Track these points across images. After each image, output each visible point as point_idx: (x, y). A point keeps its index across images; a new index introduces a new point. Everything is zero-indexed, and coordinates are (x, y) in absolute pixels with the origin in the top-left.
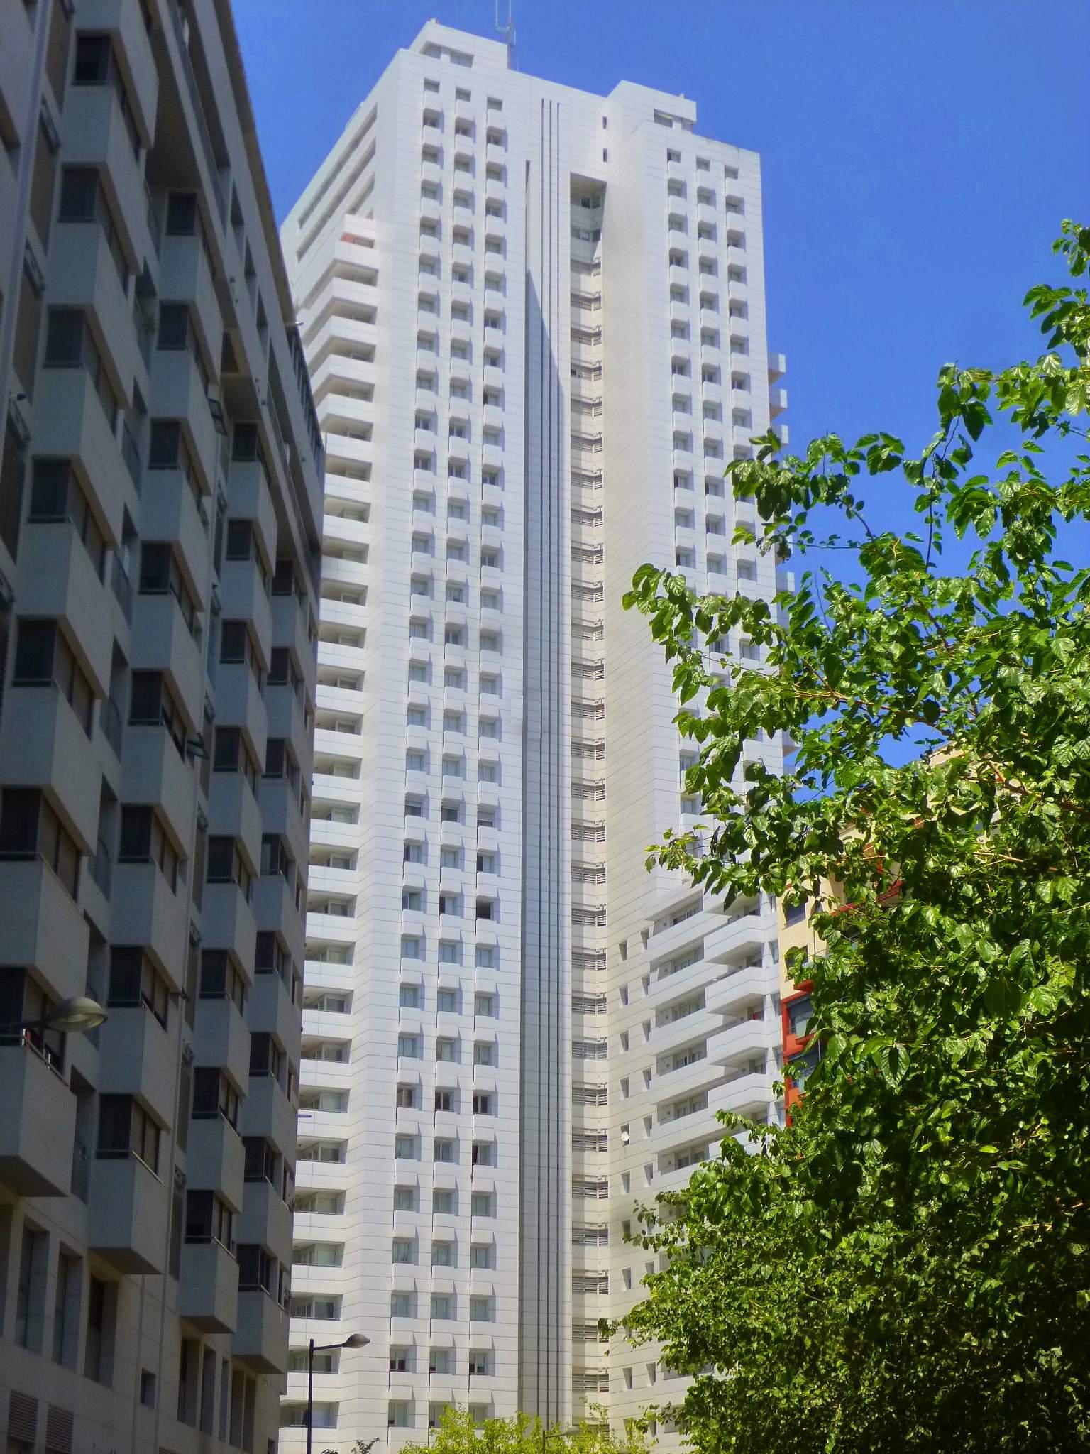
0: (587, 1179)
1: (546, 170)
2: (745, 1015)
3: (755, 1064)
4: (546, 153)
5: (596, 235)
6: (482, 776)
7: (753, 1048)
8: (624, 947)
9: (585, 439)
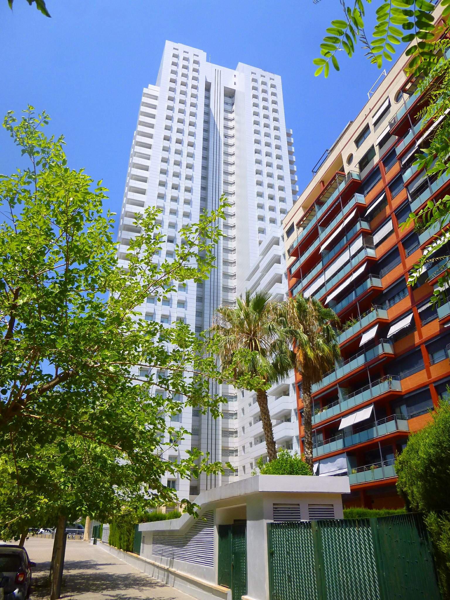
2: (282, 394)
3: (287, 418)
5: (233, 104)
8: (243, 410)
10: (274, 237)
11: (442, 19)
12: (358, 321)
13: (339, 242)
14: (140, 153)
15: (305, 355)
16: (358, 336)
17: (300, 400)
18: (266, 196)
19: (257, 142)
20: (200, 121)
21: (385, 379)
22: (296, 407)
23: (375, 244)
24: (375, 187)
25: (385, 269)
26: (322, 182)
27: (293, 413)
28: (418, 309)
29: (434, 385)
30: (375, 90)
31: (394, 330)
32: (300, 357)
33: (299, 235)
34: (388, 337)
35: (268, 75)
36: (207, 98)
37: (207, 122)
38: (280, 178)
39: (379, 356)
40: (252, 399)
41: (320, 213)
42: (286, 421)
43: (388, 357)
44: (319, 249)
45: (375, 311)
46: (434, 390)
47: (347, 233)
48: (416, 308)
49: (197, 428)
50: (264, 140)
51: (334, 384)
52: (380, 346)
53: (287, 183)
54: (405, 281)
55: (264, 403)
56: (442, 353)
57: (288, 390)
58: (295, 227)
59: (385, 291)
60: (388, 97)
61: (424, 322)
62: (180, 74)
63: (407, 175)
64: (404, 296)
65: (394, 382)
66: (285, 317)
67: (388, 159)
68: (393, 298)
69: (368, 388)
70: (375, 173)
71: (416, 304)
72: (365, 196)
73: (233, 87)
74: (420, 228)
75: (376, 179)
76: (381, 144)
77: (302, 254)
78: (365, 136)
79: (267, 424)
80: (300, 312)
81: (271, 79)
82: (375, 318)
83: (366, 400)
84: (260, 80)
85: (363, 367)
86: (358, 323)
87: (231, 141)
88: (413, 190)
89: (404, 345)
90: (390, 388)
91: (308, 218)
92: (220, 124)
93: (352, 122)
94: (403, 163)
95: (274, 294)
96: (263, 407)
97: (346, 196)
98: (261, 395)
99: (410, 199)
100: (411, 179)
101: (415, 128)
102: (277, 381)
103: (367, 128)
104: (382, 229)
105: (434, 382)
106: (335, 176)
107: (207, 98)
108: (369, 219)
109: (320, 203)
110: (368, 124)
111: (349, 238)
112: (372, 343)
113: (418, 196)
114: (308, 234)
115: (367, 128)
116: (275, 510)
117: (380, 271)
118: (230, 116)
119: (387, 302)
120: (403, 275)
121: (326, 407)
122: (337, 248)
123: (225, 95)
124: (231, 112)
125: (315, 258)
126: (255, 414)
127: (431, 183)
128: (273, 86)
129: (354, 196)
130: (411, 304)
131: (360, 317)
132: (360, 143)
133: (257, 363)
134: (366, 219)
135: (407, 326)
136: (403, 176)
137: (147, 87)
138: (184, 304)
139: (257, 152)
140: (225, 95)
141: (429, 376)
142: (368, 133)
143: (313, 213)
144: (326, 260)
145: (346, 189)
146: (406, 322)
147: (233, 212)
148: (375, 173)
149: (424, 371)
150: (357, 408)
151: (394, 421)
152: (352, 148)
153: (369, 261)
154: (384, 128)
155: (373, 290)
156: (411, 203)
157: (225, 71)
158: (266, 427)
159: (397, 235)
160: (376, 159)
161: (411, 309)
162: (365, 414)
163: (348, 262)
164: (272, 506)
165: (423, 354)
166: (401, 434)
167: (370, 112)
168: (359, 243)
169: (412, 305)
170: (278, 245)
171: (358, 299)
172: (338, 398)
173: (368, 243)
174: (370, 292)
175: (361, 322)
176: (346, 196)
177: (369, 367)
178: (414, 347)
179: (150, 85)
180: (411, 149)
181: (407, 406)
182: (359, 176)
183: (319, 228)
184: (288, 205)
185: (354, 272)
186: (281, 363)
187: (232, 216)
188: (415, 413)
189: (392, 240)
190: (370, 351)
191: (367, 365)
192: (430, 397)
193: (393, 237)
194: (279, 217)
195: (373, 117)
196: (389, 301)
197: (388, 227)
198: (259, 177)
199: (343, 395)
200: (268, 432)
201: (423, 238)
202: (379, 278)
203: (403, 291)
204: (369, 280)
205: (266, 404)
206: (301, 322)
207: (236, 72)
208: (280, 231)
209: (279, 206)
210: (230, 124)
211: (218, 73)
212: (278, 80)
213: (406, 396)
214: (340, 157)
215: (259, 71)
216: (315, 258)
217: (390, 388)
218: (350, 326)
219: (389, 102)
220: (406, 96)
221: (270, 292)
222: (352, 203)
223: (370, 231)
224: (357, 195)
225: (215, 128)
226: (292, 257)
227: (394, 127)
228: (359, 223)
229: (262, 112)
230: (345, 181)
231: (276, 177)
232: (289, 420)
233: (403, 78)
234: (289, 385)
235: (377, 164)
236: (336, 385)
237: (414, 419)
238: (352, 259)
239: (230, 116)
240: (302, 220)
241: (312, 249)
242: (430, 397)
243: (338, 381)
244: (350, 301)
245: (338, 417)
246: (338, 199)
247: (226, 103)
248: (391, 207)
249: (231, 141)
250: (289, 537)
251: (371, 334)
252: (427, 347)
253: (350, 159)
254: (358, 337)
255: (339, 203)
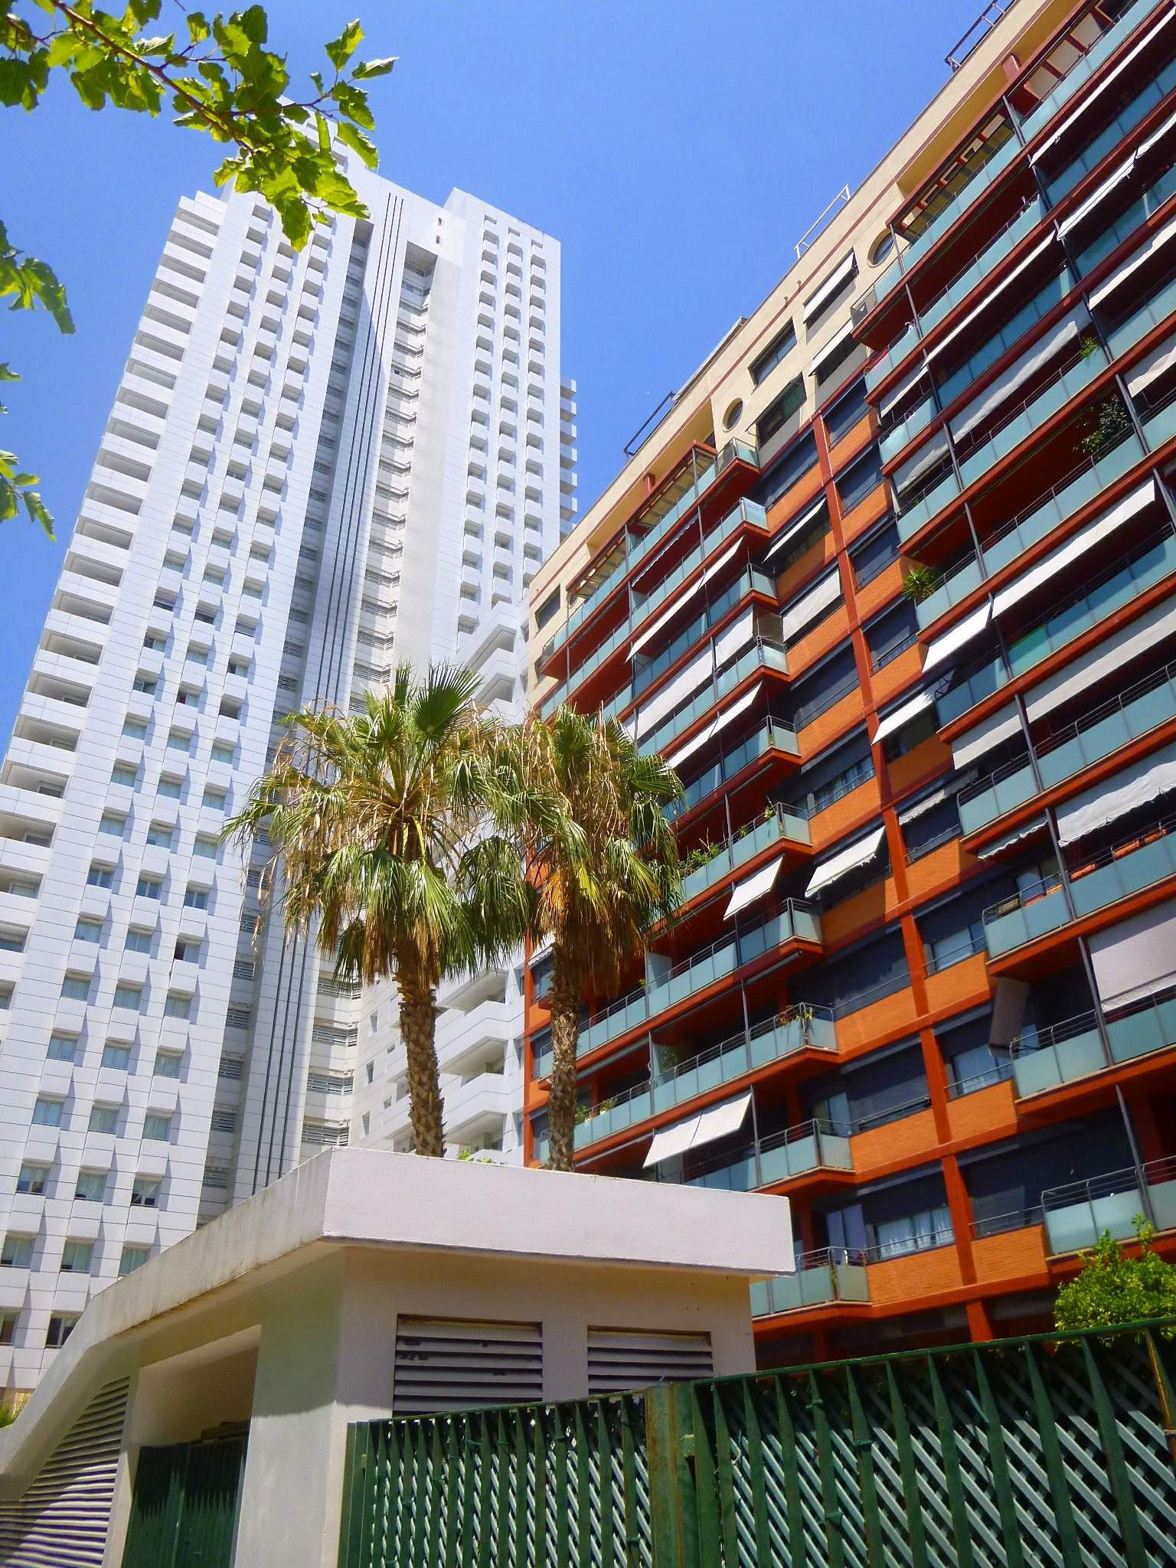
0: (336, 1025)
1: (325, 672)
2: (481, 1142)
3: (493, 1064)
4: (325, 672)
5: (426, 292)
6: (159, 1070)
7: (485, 1113)
8: (366, 1119)
9: (380, 606)
10: (500, 629)
11: (1010, 54)
12: (722, 848)
13: (686, 629)
14: (145, 366)
15: (572, 890)
16: (721, 891)
17: (534, 1085)
18: (489, 535)
19: (481, 392)
20: (331, 309)
21: (791, 1016)
22: (519, 1104)
23: (785, 639)
24: (794, 489)
25: (812, 706)
26: (651, 476)
27: (510, 1125)
28: (899, 815)
29: (933, 1032)
30: (814, 239)
31: (824, 875)
32: (555, 900)
33: (571, 617)
34: (807, 895)
35: (529, 232)
36: (358, 261)
37: (348, 323)
38: (533, 495)
39: (778, 948)
40: (395, 1086)
41: (636, 554)
42: (486, 1147)
43: (806, 952)
44: (626, 649)
45: (775, 820)
46: (935, 1046)
47: (712, 603)
48: (895, 813)
49: (223, 1165)
50: (494, 496)
51: (639, 1032)
52: (784, 917)
53: (550, 483)
54: (866, 735)
55: (421, 1031)
56: (963, 939)
57: (501, 1058)
58: (564, 594)
59: (808, 767)
60: (852, 250)
61: (914, 853)
62: (299, 283)
63: (894, 444)
64: (862, 780)
65: (817, 1023)
66: (517, 769)
67: (836, 414)
68: (829, 787)
69: (741, 1042)
70: (803, 447)
71: (895, 799)
72: (767, 511)
73: (431, 247)
74: (923, 585)
75: (801, 463)
76: (823, 372)
77: (576, 665)
78: (780, 354)
79: (426, 1102)
80: (565, 758)
81: (533, 243)
82: (775, 837)
83: (730, 1078)
84: (506, 240)
85: (730, 981)
86: (724, 855)
87: (409, 385)
88: (906, 483)
89: (852, 919)
90: (807, 1042)
91: (602, 572)
92: (387, 337)
93: (744, 321)
94: (884, 413)
95: (488, 679)
96: (417, 1042)
97: (716, 507)
98: (415, 1005)
99: (897, 509)
100: (903, 454)
101: (924, 320)
102: (473, 964)
103: (788, 332)
104: (807, 599)
105: (936, 1025)
106: (691, 452)
107: (358, 261)
108: (775, 569)
109: (637, 527)
110: (791, 322)
111: (714, 620)
112: (761, 912)
113: (921, 498)
114: (599, 611)
115: (788, 332)
116: (408, 1350)
117: (795, 710)
118: (416, 321)
119: (811, 797)
120: (864, 720)
121: (611, 1101)
122: (679, 647)
123: (407, 265)
124: (420, 312)
125: (616, 675)
126: (398, 1133)
127: (961, 463)
128: (537, 262)
129: (738, 504)
130: (878, 802)
131: (731, 838)
132: (764, 374)
133: (411, 886)
134: (765, 569)
135: (867, 860)
136: (881, 447)
137: (192, 197)
138: (223, 798)
139: (478, 418)
140: (408, 265)
141: (922, 1005)
142: (790, 343)
143: (618, 556)
144: (643, 682)
145: (716, 489)
146: (864, 851)
147: (393, 571)
148: (803, 447)
149: (909, 991)
150: (700, 1103)
151: (810, 1140)
152: (741, 385)
153: (767, 678)
154: (839, 325)
155: (774, 759)
156: (900, 517)
157: (415, 204)
158: (423, 1112)
159: (852, 612)
160: (807, 412)
161: (880, 815)
162: (729, 1119)
163: (708, 683)
164: (390, 1328)
165: (907, 944)
166: (830, 1177)
167: (800, 290)
168: (743, 630)
169: (882, 805)
170: (509, 699)
171: (730, 787)
172: (647, 1075)
173: (768, 630)
174: (765, 765)
175: (731, 853)
176: (716, 507)
177: (745, 980)
178: (881, 922)
179: (200, 194)
180: (907, 377)
181: (849, 1099)
182: (756, 455)
183: (632, 595)
184: (547, 538)
185: (723, 711)
186: (492, 906)
187: (389, 580)
188: (873, 1116)
189: (838, 625)
190: (750, 935)
191: (741, 974)
192: (920, 1070)
193: (841, 617)
194: (521, 566)
195: (806, 304)
196: (817, 797)
197: (830, 589)
198: (475, 485)
199: (662, 1066)
200: (428, 1128)
201: (929, 611)
202: (791, 730)
203: (859, 765)
204: (764, 733)
205: (430, 1035)
206: (567, 788)
207: (442, 212)
208: (518, 615)
209: (522, 537)
210: (414, 341)
211: (394, 207)
212: (552, 249)
213: (850, 1068)
214: (706, 409)
215: (504, 221)
216: (616, 675)
217: (807, 1042)
218: (697, 865)
219: (854, 262)
220: (901, 242)
221: (482, 671)
222: (730, 524)
223: (775, 603)
224: (746, 503)
225: (372, 342)
226: (548, 678)
227: (866, 319)
228: (746, 575)
229: (499, 391)
230: (717, 466)
231: (521, 490)
232: (497, 1146)
233: (895, 200)
234: (505, 1042)
235: (809, 425)
236: (644, 1035)
237: (871, 1133)
238: (719, 675)
239: (416, 321)
240: (583, 574)
241: (605, 653)
242: (920, 1070)
243: (652, 1025)
244: (705, 792)
245: (642, 1129)
246: (692, 513)
247: (406, 285)
248: (838, 538)
249: (409, 385)
250: (471, 1509)
251: (763, 882)
252: (920, 923)
253: (733, 414)
254: (722, 894)
255: (695, 526)
